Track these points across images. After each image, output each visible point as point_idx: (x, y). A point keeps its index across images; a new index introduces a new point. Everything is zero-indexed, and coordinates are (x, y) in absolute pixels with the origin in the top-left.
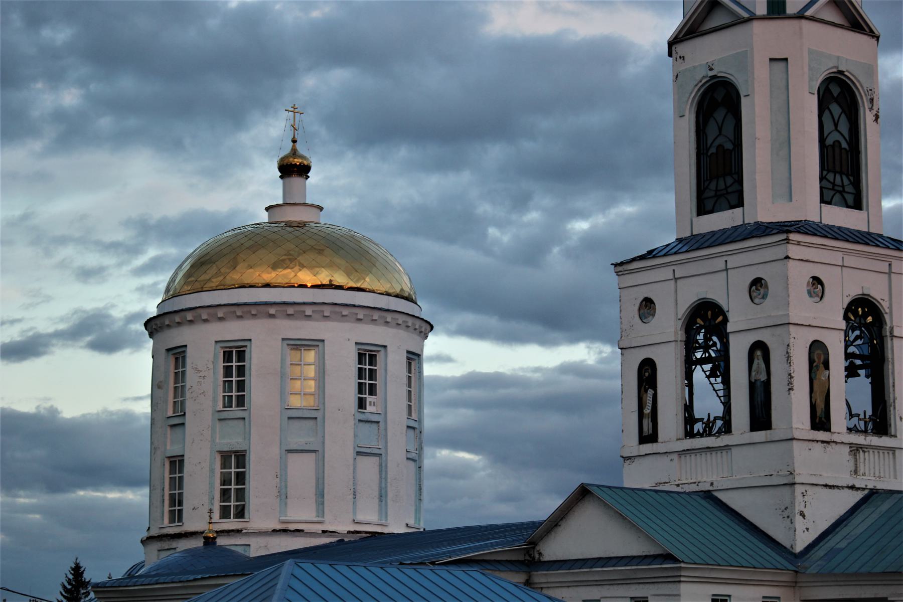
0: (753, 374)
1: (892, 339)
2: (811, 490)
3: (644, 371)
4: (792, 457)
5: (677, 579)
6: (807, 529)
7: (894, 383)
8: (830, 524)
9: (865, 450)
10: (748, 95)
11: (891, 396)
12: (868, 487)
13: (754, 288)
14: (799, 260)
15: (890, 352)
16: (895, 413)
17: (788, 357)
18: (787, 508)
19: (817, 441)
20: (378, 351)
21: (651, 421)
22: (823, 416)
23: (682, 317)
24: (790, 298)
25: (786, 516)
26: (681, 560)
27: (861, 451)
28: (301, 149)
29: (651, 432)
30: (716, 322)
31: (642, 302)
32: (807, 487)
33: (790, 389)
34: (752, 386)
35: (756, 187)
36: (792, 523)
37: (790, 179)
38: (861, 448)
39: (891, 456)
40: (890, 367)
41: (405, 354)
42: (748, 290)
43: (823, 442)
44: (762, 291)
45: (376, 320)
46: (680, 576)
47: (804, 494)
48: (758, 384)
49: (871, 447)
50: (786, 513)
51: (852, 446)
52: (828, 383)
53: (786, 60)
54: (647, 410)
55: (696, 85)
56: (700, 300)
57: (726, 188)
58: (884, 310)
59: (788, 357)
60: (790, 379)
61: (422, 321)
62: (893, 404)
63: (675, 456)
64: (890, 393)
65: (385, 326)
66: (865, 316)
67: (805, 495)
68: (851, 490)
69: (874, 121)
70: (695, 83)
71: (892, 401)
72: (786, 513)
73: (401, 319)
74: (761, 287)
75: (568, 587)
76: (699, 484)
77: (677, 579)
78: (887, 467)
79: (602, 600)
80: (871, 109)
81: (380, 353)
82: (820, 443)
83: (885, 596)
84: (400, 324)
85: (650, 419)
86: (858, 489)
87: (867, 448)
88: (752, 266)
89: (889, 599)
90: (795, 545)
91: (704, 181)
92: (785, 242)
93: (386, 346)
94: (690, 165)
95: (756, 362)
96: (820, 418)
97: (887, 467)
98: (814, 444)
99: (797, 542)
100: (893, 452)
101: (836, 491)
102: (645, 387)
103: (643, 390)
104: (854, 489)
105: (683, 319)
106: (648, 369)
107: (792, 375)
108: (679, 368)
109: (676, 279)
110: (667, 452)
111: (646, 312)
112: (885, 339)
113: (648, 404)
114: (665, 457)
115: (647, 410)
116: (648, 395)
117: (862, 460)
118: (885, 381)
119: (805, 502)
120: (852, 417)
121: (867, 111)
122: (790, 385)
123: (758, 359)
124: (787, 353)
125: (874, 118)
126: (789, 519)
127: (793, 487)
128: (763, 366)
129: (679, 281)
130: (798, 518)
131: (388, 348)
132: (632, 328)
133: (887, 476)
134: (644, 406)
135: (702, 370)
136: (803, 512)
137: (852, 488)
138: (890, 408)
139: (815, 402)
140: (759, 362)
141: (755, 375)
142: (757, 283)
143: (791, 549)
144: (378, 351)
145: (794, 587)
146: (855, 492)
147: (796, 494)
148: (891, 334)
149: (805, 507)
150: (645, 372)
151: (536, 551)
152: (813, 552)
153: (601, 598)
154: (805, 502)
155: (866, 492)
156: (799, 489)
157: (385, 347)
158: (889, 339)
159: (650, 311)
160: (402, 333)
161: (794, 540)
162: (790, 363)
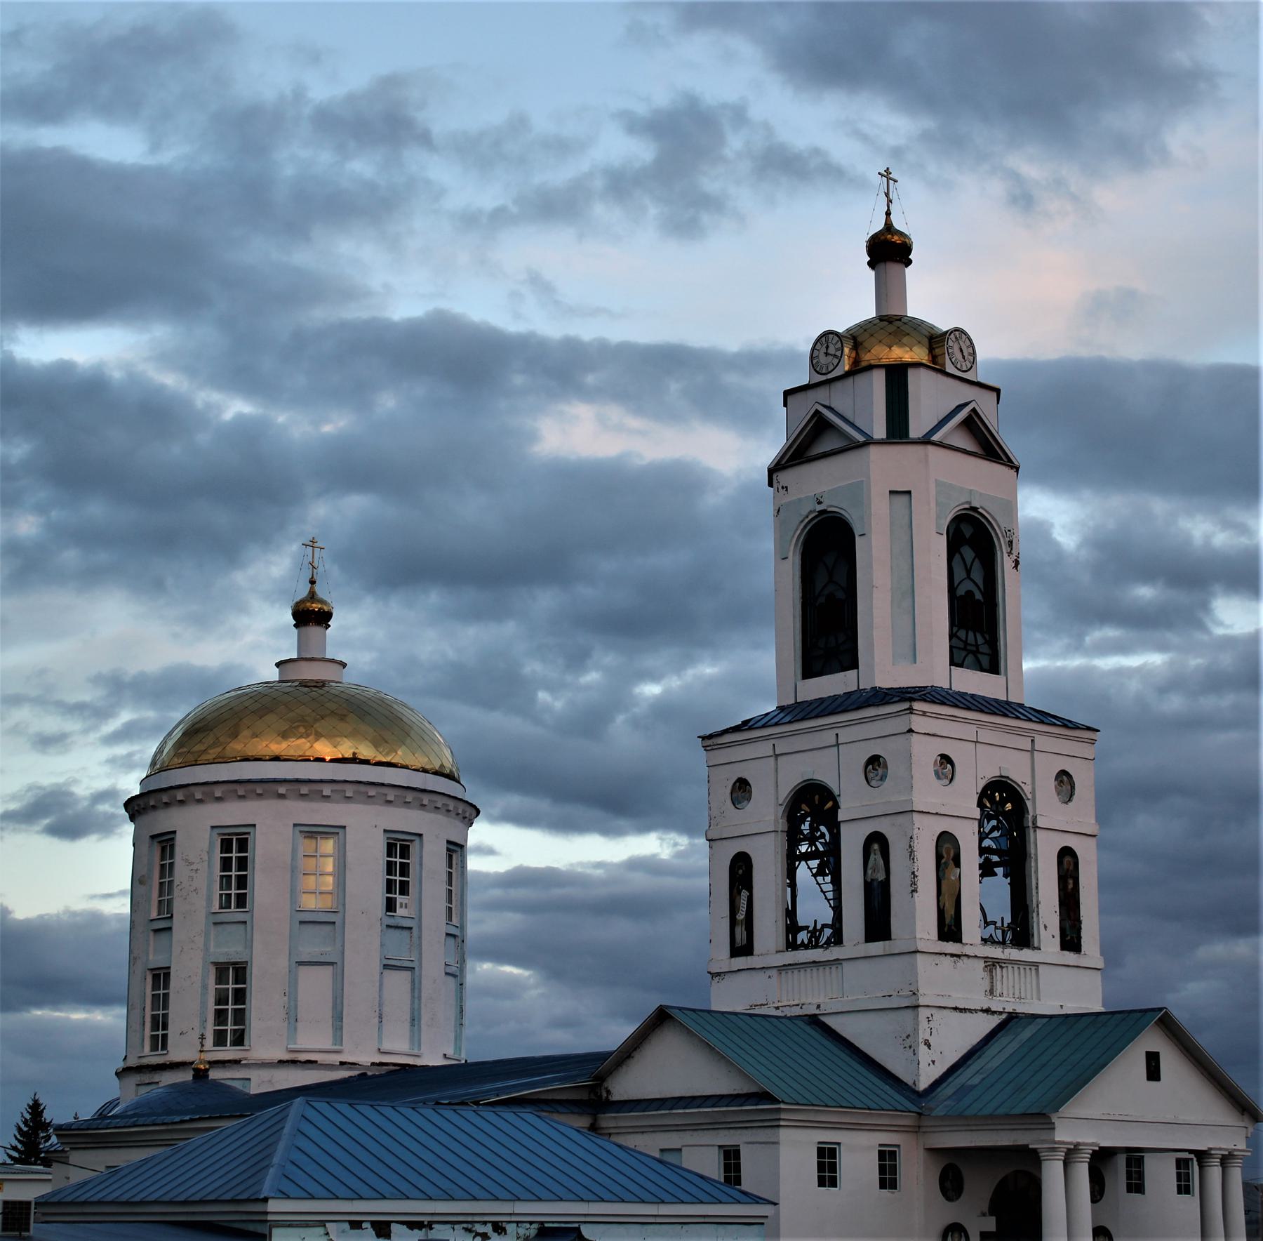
0: (869, 872)
1: (1035, 831)
2: (938, 1014)
7: (1037, 884)
9: (1003, 965)
10: (864, 534)
13: (870, 767)
14: (925, 734)
15: (1032, 846)
17: (911, 852)
19: (946, 954)
20: (412, 841)
21: (746, 929)
25: (907, 1046)
27: (998, 967)
28: (321, 591)
29: (744, 942)
32: (934, 1011)
33: (913, 891)
36: (914, 1054)
38: (998, 963)
39: (1034, 972)
40: (1033, 864)
41: (445, 845)
44: (880, 771)
48: (875, 884)
53: (909, 492)
54: (741, 916)
55: (802, 521)
58: (1025, 794)
66: (1003, 802)
68: (985, 1014)
70: (801, 519)
71: (1035, 905)
76: (803, 1007)
79: (684, 1149)
80: (1010, 553)
82: (948, 957)
84: (439, 808)
86: (994, 1013)
87: (1005, 963)
89: (1030, 1146)
90: (919, 1081)
95: (872, 857)
98: (942, 958)
101: (968, 1015)
103: (735, 891)
107: (916, 873)
109: (777, 756)
110: (764, 968)
114: (761, 973)
115: (741, 916)
116: (742, 897)
120: (987, 925)
121: (1005, 555)
123: (875, 854)
124: (910, 846)
126: (912, 1049)
128: (881, 862)
129: (779, 758)
130: (923, 1048)
132: (723, 815)
134: (736, 910)
136: (928, 1041)
140: (876, 858)
142: (874, 761)
143: (914, 1087)
146: (990, 1017)
148: (1033, 824)
151: (603, 1088)
155: (1004, 1016)
156: (923, 1013)
158: (1031, 831)
160: (440, 818)
161: (918, 1075)
162: (913, 859)
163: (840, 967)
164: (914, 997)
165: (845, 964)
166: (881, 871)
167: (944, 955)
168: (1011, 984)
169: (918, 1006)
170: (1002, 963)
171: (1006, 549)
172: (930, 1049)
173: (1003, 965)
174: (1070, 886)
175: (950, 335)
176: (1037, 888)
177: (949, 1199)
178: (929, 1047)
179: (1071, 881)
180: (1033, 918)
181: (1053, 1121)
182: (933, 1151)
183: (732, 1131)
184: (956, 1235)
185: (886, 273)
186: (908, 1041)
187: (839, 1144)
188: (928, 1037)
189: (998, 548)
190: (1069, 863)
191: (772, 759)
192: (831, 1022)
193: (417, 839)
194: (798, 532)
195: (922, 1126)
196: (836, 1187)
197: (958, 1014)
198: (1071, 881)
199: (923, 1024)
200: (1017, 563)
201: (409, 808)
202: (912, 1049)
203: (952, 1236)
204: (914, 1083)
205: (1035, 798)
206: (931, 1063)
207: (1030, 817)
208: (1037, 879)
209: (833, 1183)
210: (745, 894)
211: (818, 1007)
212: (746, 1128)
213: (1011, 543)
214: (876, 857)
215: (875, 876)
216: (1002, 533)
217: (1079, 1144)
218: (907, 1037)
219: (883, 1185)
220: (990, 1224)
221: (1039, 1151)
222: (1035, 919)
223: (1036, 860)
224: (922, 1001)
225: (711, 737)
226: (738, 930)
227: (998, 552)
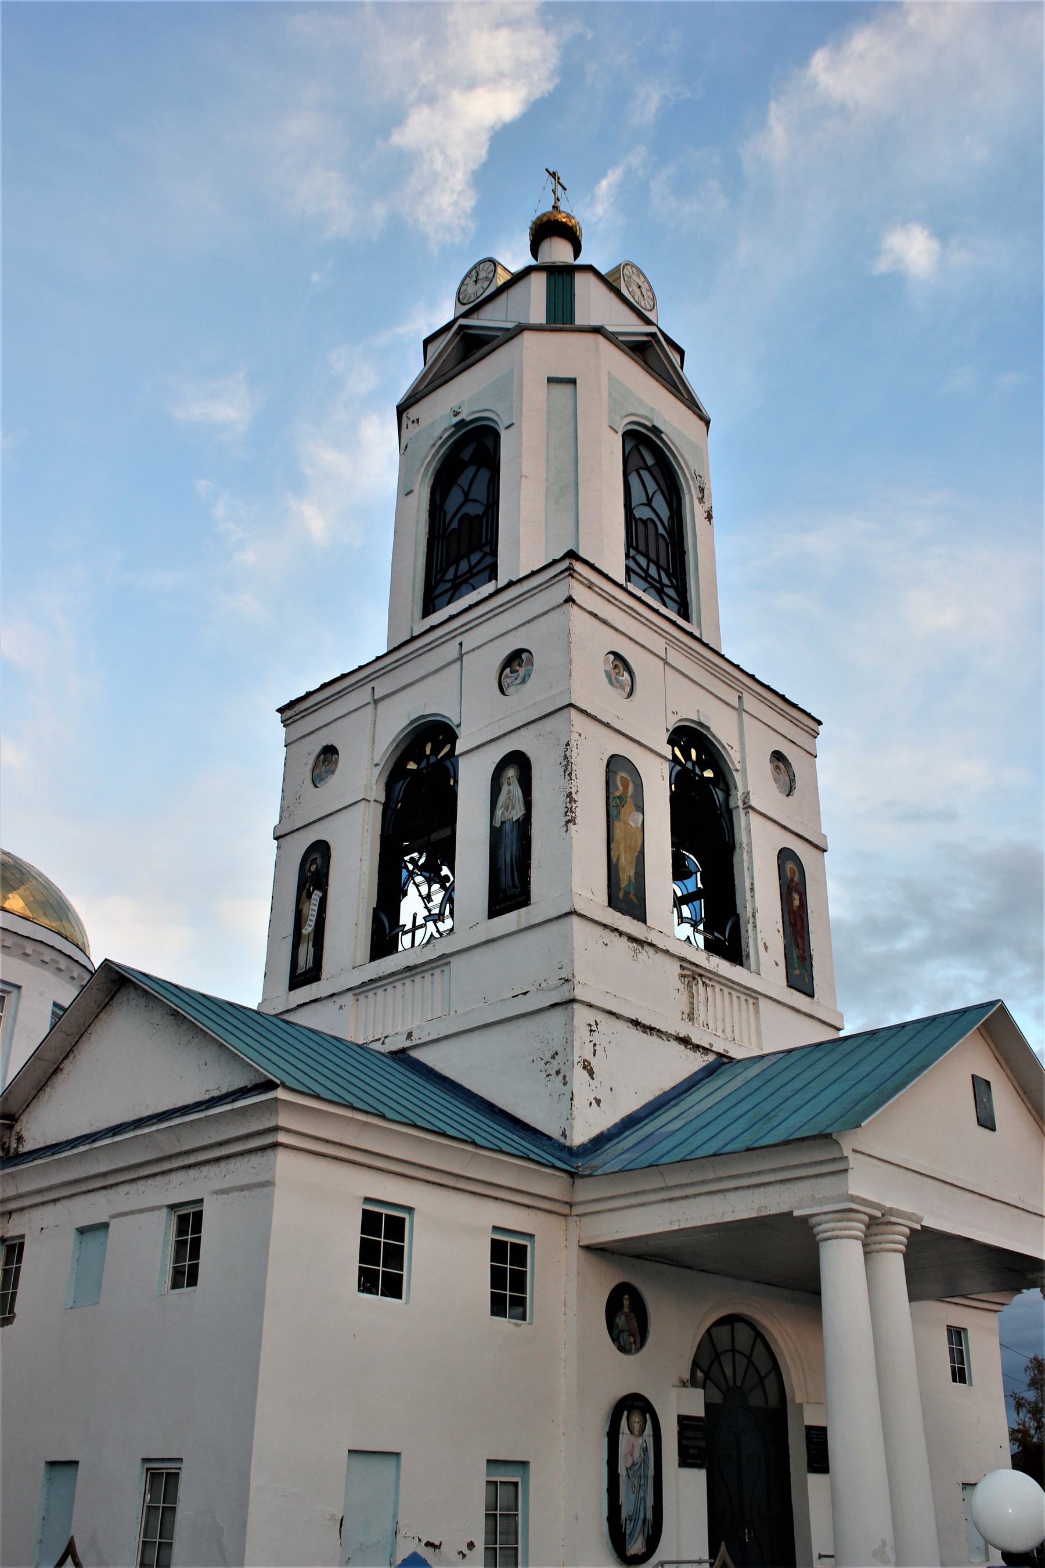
0: (499, 812)
1: (747, 813)
2: (606, 1024)
3: (309, 862)
4: (570, 952)
5: (268, 1140)
6: (598, 1102)
7: (752, 884)
8: (643, 1103)
9: (707, 981)
10: (512, 424)
11: (749, 905)
12: (713, 1049)
13: (508, 670)
14: (591, 613)
15: (744, 833)
16: (755, 939)
17: (566, 766)
18: (556, 1053)
19: (621, 933)
20: (9, 992)
21: (313, 946)
22: (632, 891)
23: (381, 759)
24: (573, 664)
25: (553, 1072)
26: (278, 1082)
27: (700, 983)
29: (310, 964)
30: (439, 757)
31: (318, 757)
32: (601, 1017)
33: (568, 822)
34: (496, 835)
35: (519, 541)
36: (565, 1084)
37: (577, 536)
38: (701, 976)
39: (751, 1007)
40: (745, 857)
41: (50, 1007)
42: (499, 671)
43: (632, 939)
44: (522, 671)
45: (9, 948)
46: (276, 1129)
47: (593, 1028)
48: (508, 827)
49: (718, 979)
50: (554, 1065)
51: (684, 964)
52: (640, 836)
53: (573, 381)
54: (308, 929)
55: (434, 445)
56: (412, 723)
57: (471, 568)
58: (733, 763)
59: (566, 766)
60: (570, 802)
61: (82, 969)
62: (751, 921)
63: (348, 999)
64: (746, 901)
65: (22, 959)
67: (594, 1031)
68: (683, 1047)
69: (705, 518)
70: (432, 443)
71: (749, 914)
72: (554, 1065)
73: (48, 955)
74: (520, 665)
75: (55, 1201)
76: (387, 1041)
77: (268, 1140)
78: (744, 1024)
79: (113, 1224)
80: (701, 500)
81: (10, 995)
82: (624, 939)
83: (784, 1209)
84: (47, 963)
85: (311, 943)
86: (696, 1047)
88: (506, 636)
89: (796, 1213)
90: (572, 1128)
91: (437, 573)
92: (567, 573)
93: (21, 987)
94: (416, 554)
95: (505, 789)
96: (627, 893)
97: (744, 1024)
98: (614, 937)
99: (575, 1123)
100: (754, 1001)
101: (654, 1039)
102: (309, 889)
103: (304, 894)
104: (689, 1047)
105: (382, 765)
106: (316, 858)
107: (574, 795)
108: (367, 847)
109: (376, 702)
110: (333, 995)
111: (323, 769)
112: (734, 813)
113: (310, 917)
114: (329, 1004)
115: (308, 929)
116: (312, 901)
117: (702, 998)
118: (737, 882)
119: (595, 1045)
120: (682, 922)
121: (696, 502)
122: (569, 813)
123: (509, 784)
124: (566, 757)
125: (706, 515)
126: (561, 1076)
127: (569, 1009)
128: (518, 792)
129: (380, 705)
130: (579, 1075)
131: (23, 989)
132: (298, 801)
133: (745, 1040)
134: (303, 921)
135: (418, 894)
136: (589, 1063)
137: (685, 1041)
138: (746, 926)
139: (618, 860)
140: (512, 790)
141: (503, 813)
142: (516, 659)
143: (562, 1140)
144: (9, 992)
145: (565, 1216)
146: (689, 1053)
147: (576, 1022)
148: (744, 803)
149: (594, 1054)
150: (311, 865)
151: (14, 1133)
152: (608, 1146)
153: (112, 1217)
154: (595, 1045)
155: (711, 1058)
156: (582, 1016)
157: (19, 987)
158: (742, 812)
159: (330, 767)
160: (48, 976)
161: (570, 1118)
162: (570, 774)
163: (445, 968)
164: (567, 986)
165: (452, 960)
166: (517, 806)
167: (617, 934)
168: (719, 1016)
169: (573, 1001)
170: (707, 977)
171: (696, 494)
172: (593, 1078)
173: (710, 983)
174: (796, 903)
175: (623, 270)
176: (752, 890)
177: (623, 1349)
178: (591, 1073)
179: (796, 896)
180: (747, 931)
181: (845, 1155)
182: (596, 1250)
183: (193, 1173)
184: (636, 1418)
185: (551, 247)
186: (554, 1063)
187: (410, 1210)
188: (589, 1057)
189: (686, 491)
190: (793, 873)
191: (370, 708)
192: (426, 1057)
193: (15, 991)
194: (428, 459)
195: (576, 1204)
196: (400, 1297)
197: (637, 1034)
198: (796, 896)
199: (581, 1033)
200: (709, 517)
201: (8, 955)
202: (561, 1076)
203: (628, 1418)
204: (564, 1135)
205: (746, 770)
206: (594, 1102)
207: (739, 794)
208: (752, 878)
209: (393, 1288)
210: (317, 895)
211: (410, 1035)
212: (218, 1160)
213: (702, 490)
214: (511, 787)
215: (508, 816)
216: (691, 475)
217: (891, 1211)
218: (553, 1057)
219: (498, 1307)
220: (695, 1404)
221: (813, 1221)
222: (750, 933)
223: (750, 852)
224: (580, 993)
225: (292, 704)
226: (302, 950)
227: (686, 496)
